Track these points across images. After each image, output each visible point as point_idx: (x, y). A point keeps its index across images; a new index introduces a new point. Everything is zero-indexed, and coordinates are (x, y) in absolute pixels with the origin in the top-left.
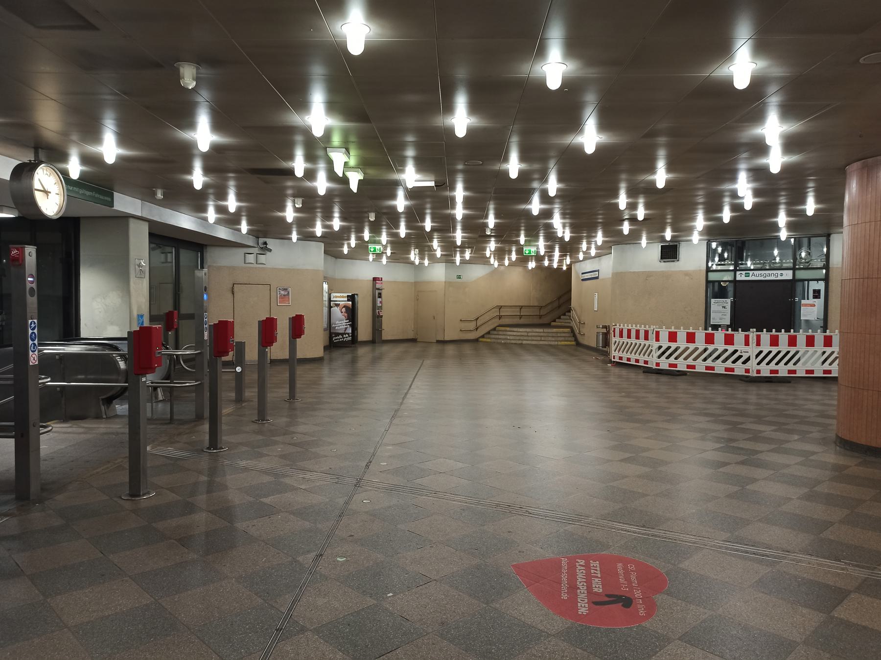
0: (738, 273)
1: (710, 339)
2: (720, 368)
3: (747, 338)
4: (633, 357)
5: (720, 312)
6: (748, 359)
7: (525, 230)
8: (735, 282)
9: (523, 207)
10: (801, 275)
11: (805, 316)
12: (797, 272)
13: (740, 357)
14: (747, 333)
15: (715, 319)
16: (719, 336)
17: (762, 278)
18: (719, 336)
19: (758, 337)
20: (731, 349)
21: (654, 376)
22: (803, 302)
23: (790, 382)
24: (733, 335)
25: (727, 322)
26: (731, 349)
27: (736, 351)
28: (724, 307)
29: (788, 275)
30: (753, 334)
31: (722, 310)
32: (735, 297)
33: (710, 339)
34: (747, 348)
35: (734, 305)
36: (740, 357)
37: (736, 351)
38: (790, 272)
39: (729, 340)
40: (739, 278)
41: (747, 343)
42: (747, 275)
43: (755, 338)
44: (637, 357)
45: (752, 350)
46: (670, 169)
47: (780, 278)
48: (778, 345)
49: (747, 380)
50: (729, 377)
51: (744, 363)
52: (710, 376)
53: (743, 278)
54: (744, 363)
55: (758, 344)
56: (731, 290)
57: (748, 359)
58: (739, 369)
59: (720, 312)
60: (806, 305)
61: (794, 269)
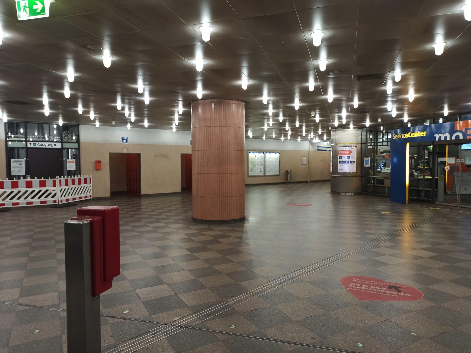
0: (28, 143)
1: (15, 185)
2: (36, 201)
3: (54, 182)
4: (77, 196)
5: (18, 167)
6: (55, 194)
7: (299, 117)
8: (27, 148)
9: (451, 111)
10: (66, 145)
11: (69, 168)
12: (64, 144)
13: (50, 194)
14: (54, 179)
15: (14, 172)
16: (22, 182)
17: (44, 147)
18: (22, 182)
19: (60, 181)
20: (44, 189)
21: (64, 209)
22: (68, 160)
23: (77, 205)
24: (45, 181)
25: (24, 174)
26: (44, 189)
27: (47, 191)
28: (21, 164)
29: (59, 145)
30: (57, 179)
31: (18, 167)
32: (27, 157)
33: (15, 185)
34: (54, 188)
35: (27, 163)
36: (50, 194)
37: (47, 191)
38: (60, 144)
39: (29, 185)
40: (29, 146)
41: (54, 185)
42: (34, 144)
43: (59, 182)
44: (73, 196)
45: (57, 189)
46: (360, 100)
47: (54, 147)
48: (18, 188)
49: (55, 207)
50: (44, 207)
51: (53, 197)
52: (30, 208)
53: (32, 146)
54: (53, 197)
55: (60, 185)
56: (23, 152)
57: (55, 194)
58: (50, 201)
59: (18, 167)
60: (70, 162)
61: (62, 142)
